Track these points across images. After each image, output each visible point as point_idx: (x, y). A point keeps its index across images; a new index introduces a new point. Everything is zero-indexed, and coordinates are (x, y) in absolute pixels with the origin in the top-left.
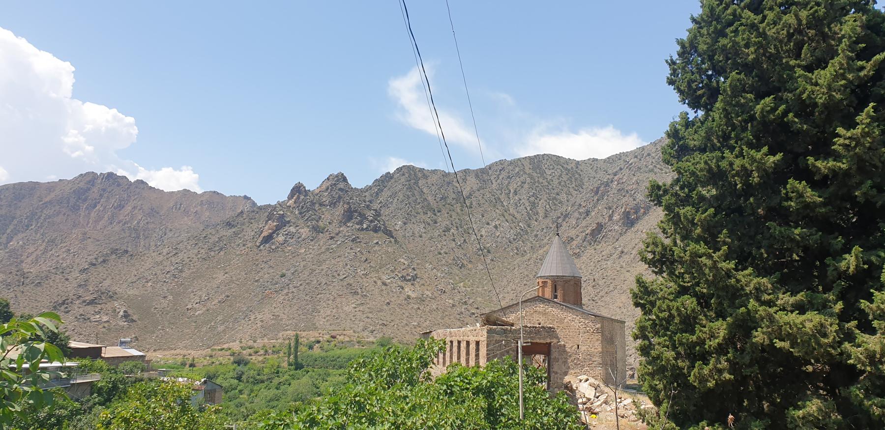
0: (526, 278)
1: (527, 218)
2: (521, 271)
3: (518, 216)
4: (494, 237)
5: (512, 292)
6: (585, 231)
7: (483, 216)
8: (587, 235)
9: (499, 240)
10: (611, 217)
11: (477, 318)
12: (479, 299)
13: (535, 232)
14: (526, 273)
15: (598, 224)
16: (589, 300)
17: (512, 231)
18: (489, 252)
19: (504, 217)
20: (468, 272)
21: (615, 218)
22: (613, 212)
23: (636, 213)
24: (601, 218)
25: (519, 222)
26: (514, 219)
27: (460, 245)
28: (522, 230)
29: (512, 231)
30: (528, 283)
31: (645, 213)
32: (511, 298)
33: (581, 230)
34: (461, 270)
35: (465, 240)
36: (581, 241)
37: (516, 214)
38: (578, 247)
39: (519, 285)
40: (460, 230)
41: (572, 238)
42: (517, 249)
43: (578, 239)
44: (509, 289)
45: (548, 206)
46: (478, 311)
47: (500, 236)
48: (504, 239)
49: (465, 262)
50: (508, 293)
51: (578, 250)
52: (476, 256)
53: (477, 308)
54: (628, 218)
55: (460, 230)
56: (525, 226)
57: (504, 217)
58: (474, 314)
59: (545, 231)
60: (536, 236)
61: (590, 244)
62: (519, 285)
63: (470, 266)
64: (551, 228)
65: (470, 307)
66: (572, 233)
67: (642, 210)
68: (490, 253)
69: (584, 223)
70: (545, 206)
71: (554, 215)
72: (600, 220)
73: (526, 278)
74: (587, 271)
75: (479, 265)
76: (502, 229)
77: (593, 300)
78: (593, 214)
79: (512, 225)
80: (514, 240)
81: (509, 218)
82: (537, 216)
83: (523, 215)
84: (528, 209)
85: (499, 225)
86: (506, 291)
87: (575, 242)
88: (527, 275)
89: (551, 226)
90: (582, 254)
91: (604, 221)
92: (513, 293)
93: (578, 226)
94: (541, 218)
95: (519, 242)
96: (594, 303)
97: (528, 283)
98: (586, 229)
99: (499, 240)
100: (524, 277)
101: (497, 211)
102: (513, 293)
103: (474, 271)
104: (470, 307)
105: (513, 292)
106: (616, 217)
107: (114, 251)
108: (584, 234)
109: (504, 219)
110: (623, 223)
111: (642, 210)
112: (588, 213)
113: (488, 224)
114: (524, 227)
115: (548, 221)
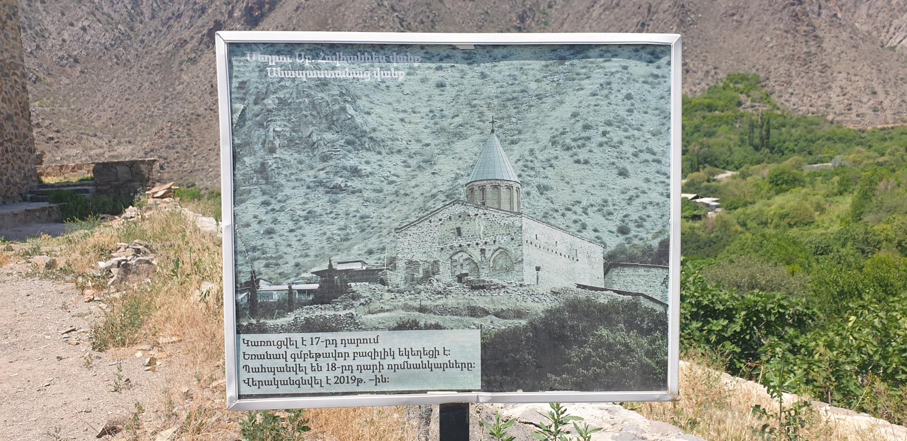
0: (128, 91)
1: (128, 19)
2: (121, 83)
3: (116, 16)
4: (83, 43)
5: (110, 109)
6: (201, 32)
7: (63, 14)
8: (204, 35)
9: (90, 46)
10: (231, 14)
11: (58, 144)
12: (62, 121)
13: (140, 37)
14: (127, 85)
15: (216, 21)
16: (206, 109)
17: (107, 34)
18: (76, 61)
19: (95, 16)
20: (47, 87)
21: (235, 15)
22: (233, 7)
23: (260, 8)
24: (220, 16)
25: (117, 24)
26: (109, 19)
27: (31, 53)
28: (123, 34)
29: (107, 34)
30: (131, 97)
31: (271, 9)
32: (109, 117)
33: (197, 30)
34: (35, 85)
35: (38, 46)
36: (197, 44)
37: (112, 14)
38: (193, 50)
39: (119, 100)
40: (29, 32)
41: (185, 41)
42: (116, 57)
43: (194, 41)
44: (106, 106)
45: (155, 5)
46: (59, 135)
47: (92, 41)
48: (98, 44)
49: (41, 75)
50: (104, 111)
51: (194, 55)
52: (58, 67)
53: (58, 131)
54: (251, 15)
55: (29, 32)
56: (127, 29)
57: (95, 16)
58: (52, 139)
59: (153, 35)
60: (142, 41)
61: (208, 47)
62: (119, 100)
63: (49, 80)
64: (160, 31)
65: (45, 131)
66: (186, 34)
67: (267, 6)
68: (78, 62)
69: (200, 22)
70: (152, 5)
71: (163, 15)
72: (219, 17)
73: (128, 91)
74: (206, 79)
75: (63, 78)
76: (93, 32)
77: (211, 110)
78: (210, 11)
79: (108, 27)
80: (112, 46)
81: (104, 18)
82: (142, 17)
83: (122, 15)
84: (129, 7)
85: (89, 26)
86: (101, 107)
87: (189, 46)
88: (130, 88)
89: (160, 28)
90: (199, 59)
91: (222, 19)
92: (112, 111)
93: (192, 26)
94: (147, 20)
95: (119, 49)
96: (212, 112)
97: (131, 97)
98: (202, 29)
99: (90, 46)
100: (126, 90)
101: (83, 7)
102: (112, 111)
103: (55, 87)
104: (45, 131)
105: (111, 109)
106: (237, 14)
107: (651, 203)
108: (200, 35)
109: (95, 19)
110: (245, 21)
111: (267, 6)
112: (203, 10)
113: (72, 25)
114: (125, 30)
115: (156, 23)
